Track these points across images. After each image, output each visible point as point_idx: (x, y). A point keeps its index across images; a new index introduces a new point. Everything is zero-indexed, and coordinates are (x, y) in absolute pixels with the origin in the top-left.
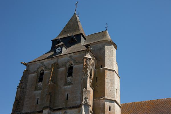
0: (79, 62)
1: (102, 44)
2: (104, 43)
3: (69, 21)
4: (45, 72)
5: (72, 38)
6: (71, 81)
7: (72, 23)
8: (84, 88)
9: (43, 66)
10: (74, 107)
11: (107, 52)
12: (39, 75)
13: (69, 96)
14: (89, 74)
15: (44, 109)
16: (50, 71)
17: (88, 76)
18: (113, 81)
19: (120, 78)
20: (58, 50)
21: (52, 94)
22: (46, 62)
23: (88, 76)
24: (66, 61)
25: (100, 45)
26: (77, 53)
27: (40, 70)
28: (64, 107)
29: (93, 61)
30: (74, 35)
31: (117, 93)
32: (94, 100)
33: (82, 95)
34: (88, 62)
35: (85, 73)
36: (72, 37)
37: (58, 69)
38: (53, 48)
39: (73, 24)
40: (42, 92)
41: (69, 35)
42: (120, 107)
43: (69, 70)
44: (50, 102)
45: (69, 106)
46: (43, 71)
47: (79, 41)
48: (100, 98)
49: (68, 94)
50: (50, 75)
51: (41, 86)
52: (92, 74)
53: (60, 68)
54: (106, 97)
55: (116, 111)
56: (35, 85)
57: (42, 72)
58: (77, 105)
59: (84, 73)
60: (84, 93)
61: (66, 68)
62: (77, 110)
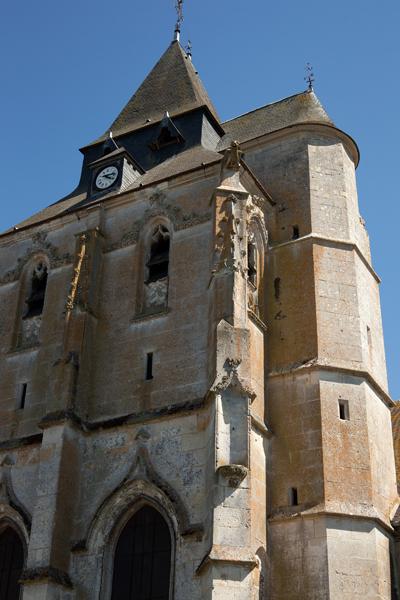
0: (194, 215)
1: (295, 140)
2: (303, 135)
3: (151, 74)
4: (54, 271)
5: (165, 129)
6: (164, 298)
7: (164, 78)
8: (222, 321)
9: (45, 250)
10: (177, 410)
11: (319, 169)
12: (29, 288)
13: (156, 362)
14: (240, 260)
15: (47, 427)
16: (71, 265)
17: (236, 265)
18: (348, 292)
19: (378, 281)
20: (106, 176)
21: (82, 362)
22: (55, 232)
23: (236, 265)
24: (139, 218)
25: (286, 146)
26: (184, 177)
27: (31, 268)
28: (137, 410)
29: (257, 210)
30: (172, 118)
31: (370, 342)
32: (271, 374)
33: (212, 353)
34: (235, 210)
35: (223, 257)
36: (164, 125)
37: (104, 253)
38: (87, 181)
39: (171, 75)
40: (39, 355)
41: (152, 121)
42: (390, 405)
43: (152, 257)
44: (74, 392)
45: (156, 406)
46: (46, 269)
47: (196, 140)
48: (296, 365)
49: (150, 356)
50: (73, 280)
51: (35, 332)
52: (257, 268)
53: (113, 249)
54: (323, 360)
55: (369, 419)
56: (12, 331)
57: (39, 273)
58: (191, 398)
59: (219, 255)
60: (219, 343)
61: (141, 247)
62: (192, 419)
